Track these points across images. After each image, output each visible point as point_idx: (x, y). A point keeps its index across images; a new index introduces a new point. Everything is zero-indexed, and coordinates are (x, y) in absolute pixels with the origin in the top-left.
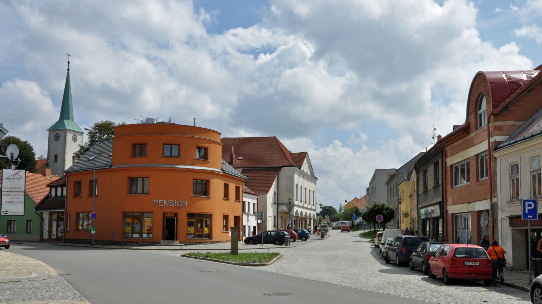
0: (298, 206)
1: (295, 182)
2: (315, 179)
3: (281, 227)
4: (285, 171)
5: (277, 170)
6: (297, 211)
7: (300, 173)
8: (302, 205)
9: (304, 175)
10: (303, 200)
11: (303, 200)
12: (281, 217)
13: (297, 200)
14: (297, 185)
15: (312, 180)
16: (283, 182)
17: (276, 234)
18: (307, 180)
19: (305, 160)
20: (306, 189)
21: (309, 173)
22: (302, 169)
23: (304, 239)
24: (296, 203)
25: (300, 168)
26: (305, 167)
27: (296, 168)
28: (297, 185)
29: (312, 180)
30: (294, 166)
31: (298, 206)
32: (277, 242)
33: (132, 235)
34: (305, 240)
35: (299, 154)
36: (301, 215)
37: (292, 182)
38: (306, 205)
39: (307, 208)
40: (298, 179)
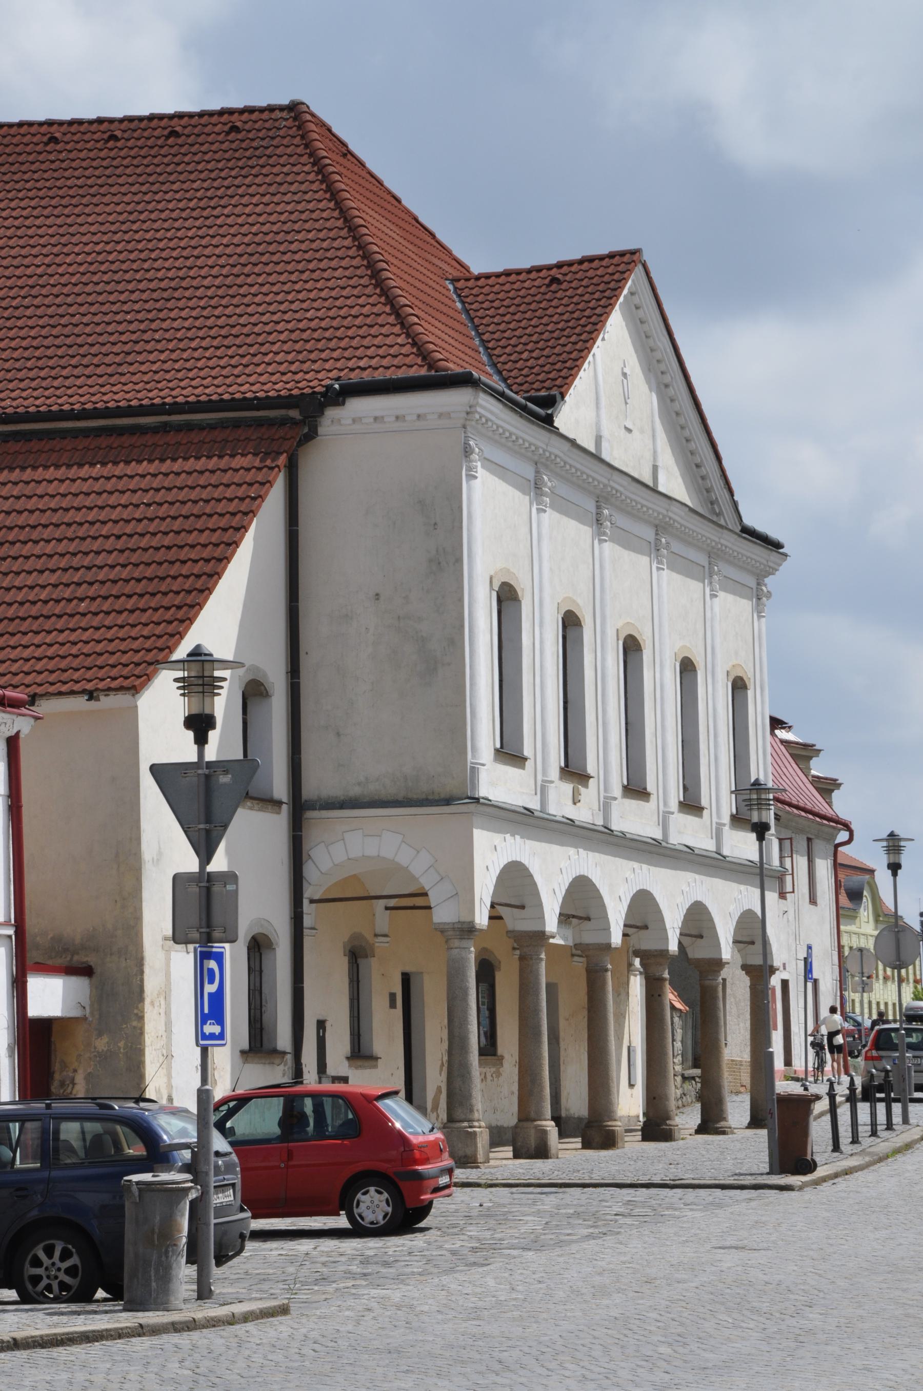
0: (526, 821)
1: (487, 555)
2: (757, 552)
3: (360, 1053)
4: (364, 441)
5: (283, 428)
6: (515, 877)
7: (541, 463)
8: (585, 812)
9: (601, 494)
10: (605, 751)
11: (605, 751)
12: (357, 955)
13: (510, 753)
14: (507, 597)
15: (714, 554)
16: (346, 562)
17: (292, 1119)
18: (654, 549)
19: (616, 325)
20: (631, 647)
21: (673, 483)
22: (572, 416)
23: (373, 1204)
24: (498, 784)
25: (541, 407)
26: (608, 397)
27: (487, 405)
28: (507, 597)
29: (714, 554)
30: (464, 381)
31: (526, 821)
32: (54, 1262)
33: (881, 1100)
34: (407, 1218)
35: (554, 276)
36: (632, 926)
37: (445, 558)
38: (634, 820)
39: (605, 839)
40: (504, 525)
